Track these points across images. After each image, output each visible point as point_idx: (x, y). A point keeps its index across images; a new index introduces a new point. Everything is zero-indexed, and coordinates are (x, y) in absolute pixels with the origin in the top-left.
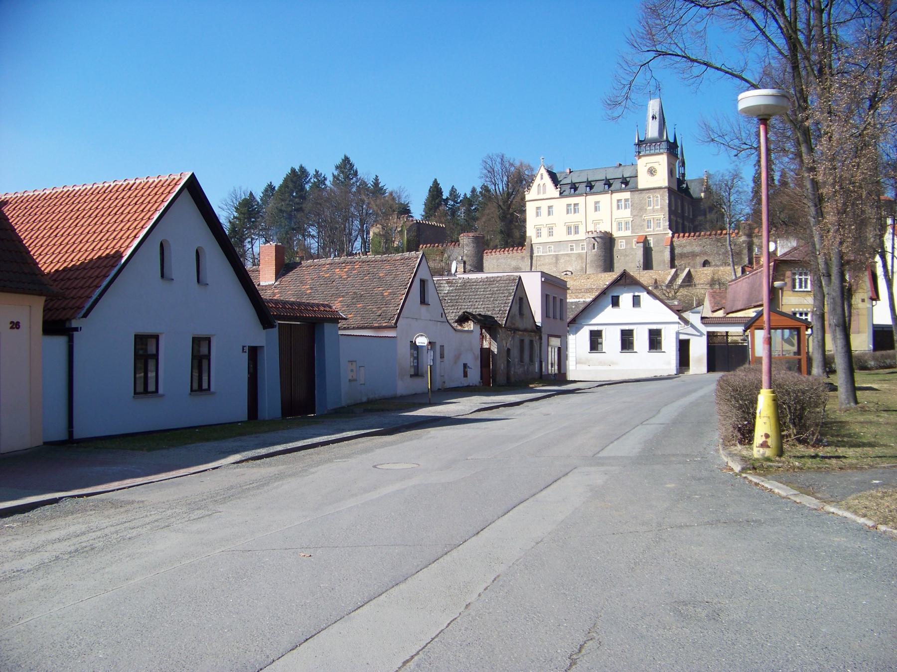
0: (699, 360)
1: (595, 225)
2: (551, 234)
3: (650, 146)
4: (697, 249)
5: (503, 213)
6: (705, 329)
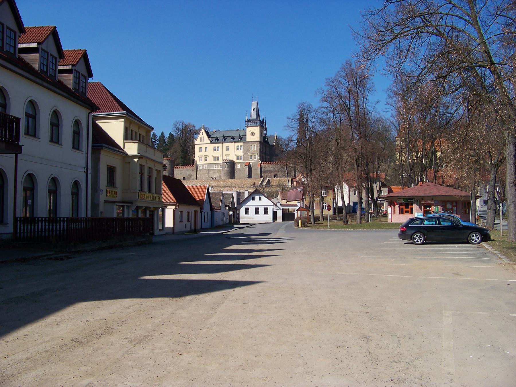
0: (280, 217)
1: (227, 156)
2: (206, 160)
3: (252, 122)
4: (272, 169)
5: (183, 149)
6: (282, 208)
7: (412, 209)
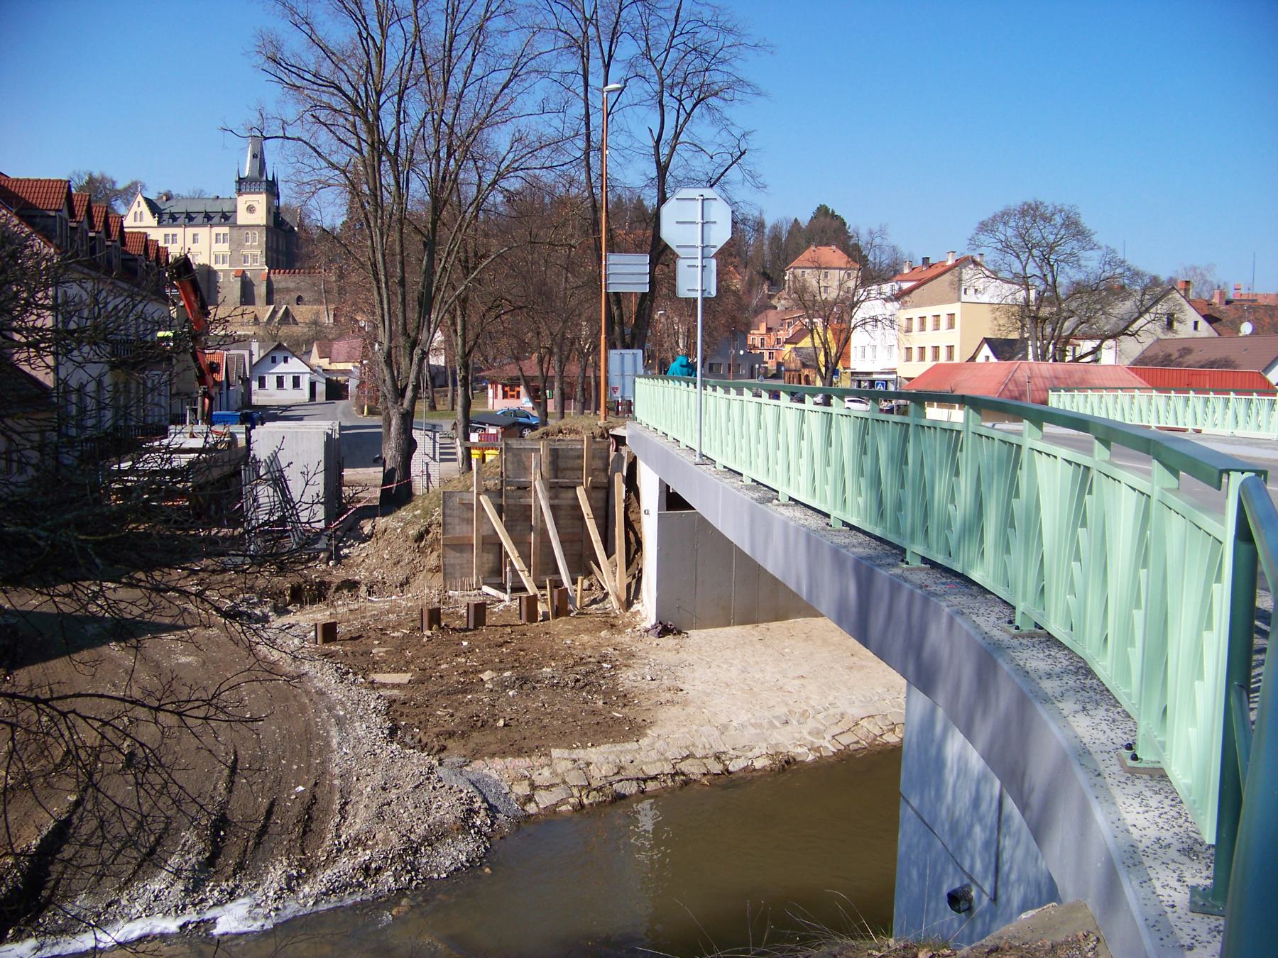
4: (292, 285)
7: (518, 392)
